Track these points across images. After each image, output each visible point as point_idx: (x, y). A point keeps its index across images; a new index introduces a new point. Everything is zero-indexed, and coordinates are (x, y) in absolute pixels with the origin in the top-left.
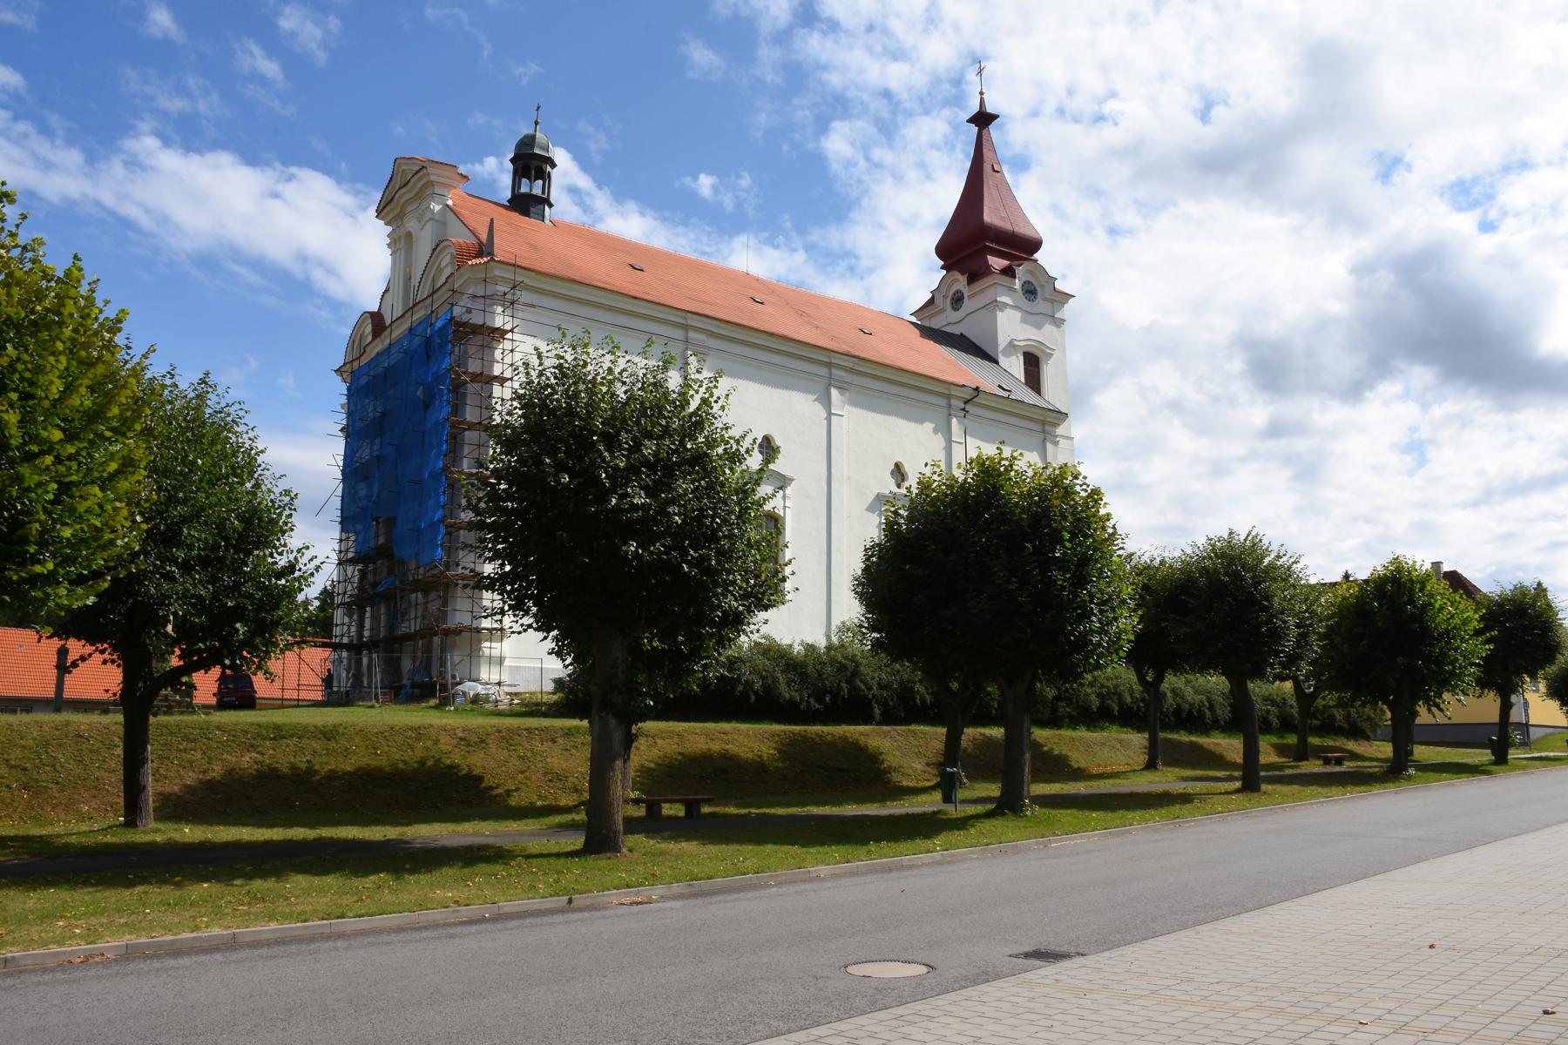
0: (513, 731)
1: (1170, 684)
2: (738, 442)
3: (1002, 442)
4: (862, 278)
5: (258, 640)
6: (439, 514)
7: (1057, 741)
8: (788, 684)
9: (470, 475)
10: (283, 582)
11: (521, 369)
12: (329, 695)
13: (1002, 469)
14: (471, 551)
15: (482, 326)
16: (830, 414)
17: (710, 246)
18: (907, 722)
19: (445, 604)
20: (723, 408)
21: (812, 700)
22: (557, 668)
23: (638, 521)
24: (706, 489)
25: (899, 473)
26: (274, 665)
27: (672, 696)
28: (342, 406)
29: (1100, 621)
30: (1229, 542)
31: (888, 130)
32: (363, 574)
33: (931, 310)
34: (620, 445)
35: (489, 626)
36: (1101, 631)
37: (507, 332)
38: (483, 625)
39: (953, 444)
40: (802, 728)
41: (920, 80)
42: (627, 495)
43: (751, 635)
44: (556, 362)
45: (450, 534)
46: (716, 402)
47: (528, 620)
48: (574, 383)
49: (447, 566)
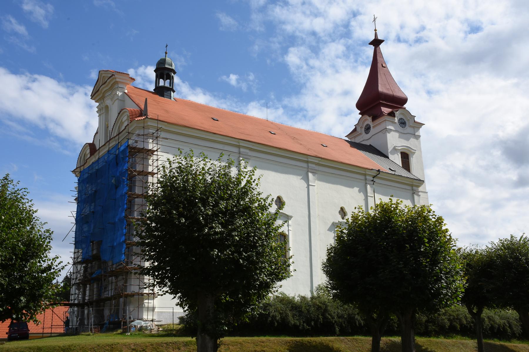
0: (159, 345)
1: (486, 314)
2: (265, 200)
3: (392, 196)
4: (310, 121)
5: (31, 305)
6: (123, 238)
7: (429, 343)
8: (293, 317)
9: (138, 220)
10: (45, 275)
11: (161, 169)
12: (67, 330)
13: (392, 209)
14: (138, 256)
15: (143, 149)
16: (308, 185)
17: (237, 108)
18: (352, 334)
19: (126, 282)
20: (257, 185)
21: (305, 325)
22: (180, 312)
23: (218, 239)
24: (250, 223)
25: (343, 212)
26: (39, 317)
27: (236, 324)
28: (76, 188)
29: (446, 282)
30: (511, 241)
31: (315, 50)
32: (86, 269)
33: (355, 134)
34: (209, 204)
35: (147, 292)
36: (447, 288)
37: (154, 151)
38: (145, 292)
39: (368, 197)
40: (301, 338)
41: (329, 26)
42: (212, 227)
43: (274, 293)
44: (177, 165)
45: (128, 248)
46: (254, 182)
47: (166, 289)
48: (187, 175)
49: (127, 264)
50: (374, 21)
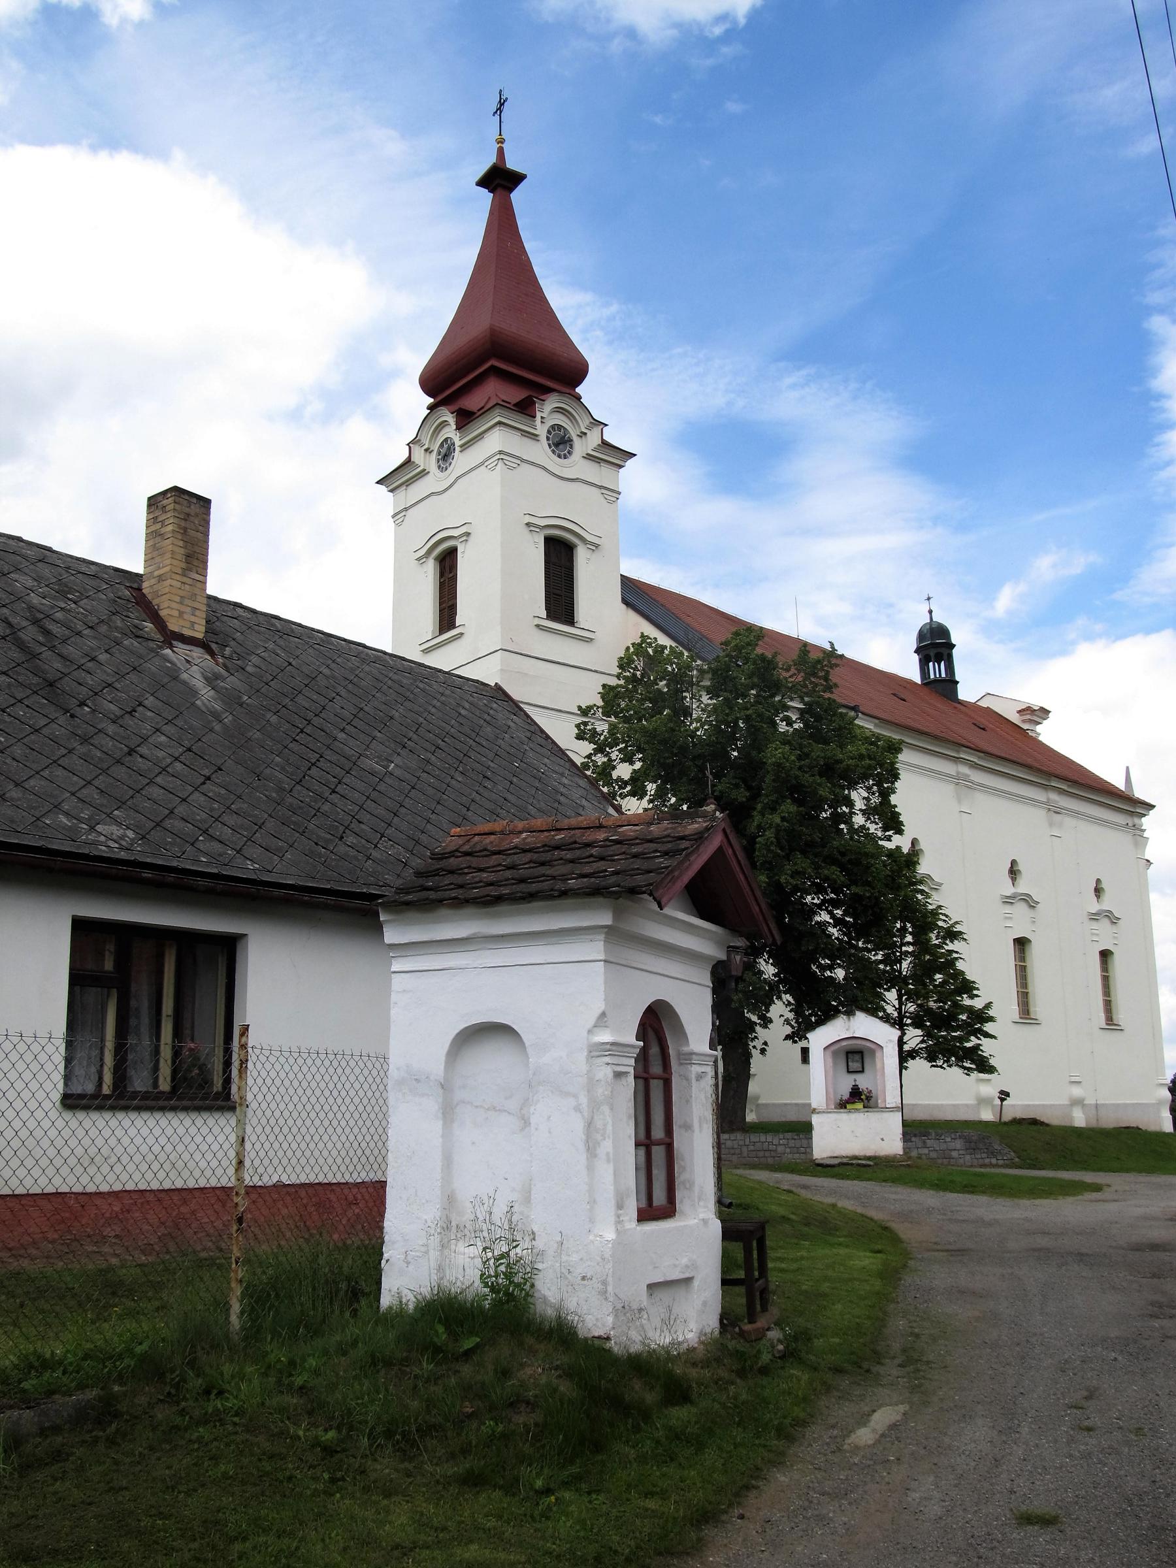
50: (502, 101)
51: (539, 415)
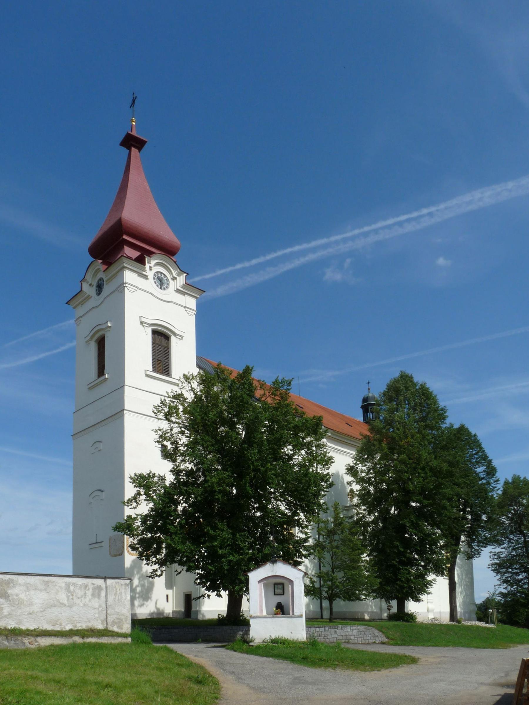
51: (147, 266)
